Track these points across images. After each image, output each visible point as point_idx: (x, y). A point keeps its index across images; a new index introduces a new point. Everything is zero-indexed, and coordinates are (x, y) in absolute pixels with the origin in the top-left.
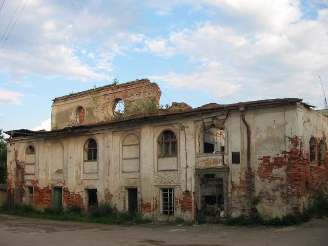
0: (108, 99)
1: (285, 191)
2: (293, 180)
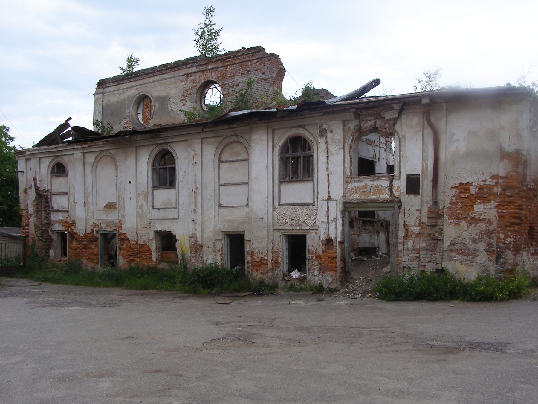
0: (193, 81)
1: (494, 241)
2: (508, 224)
